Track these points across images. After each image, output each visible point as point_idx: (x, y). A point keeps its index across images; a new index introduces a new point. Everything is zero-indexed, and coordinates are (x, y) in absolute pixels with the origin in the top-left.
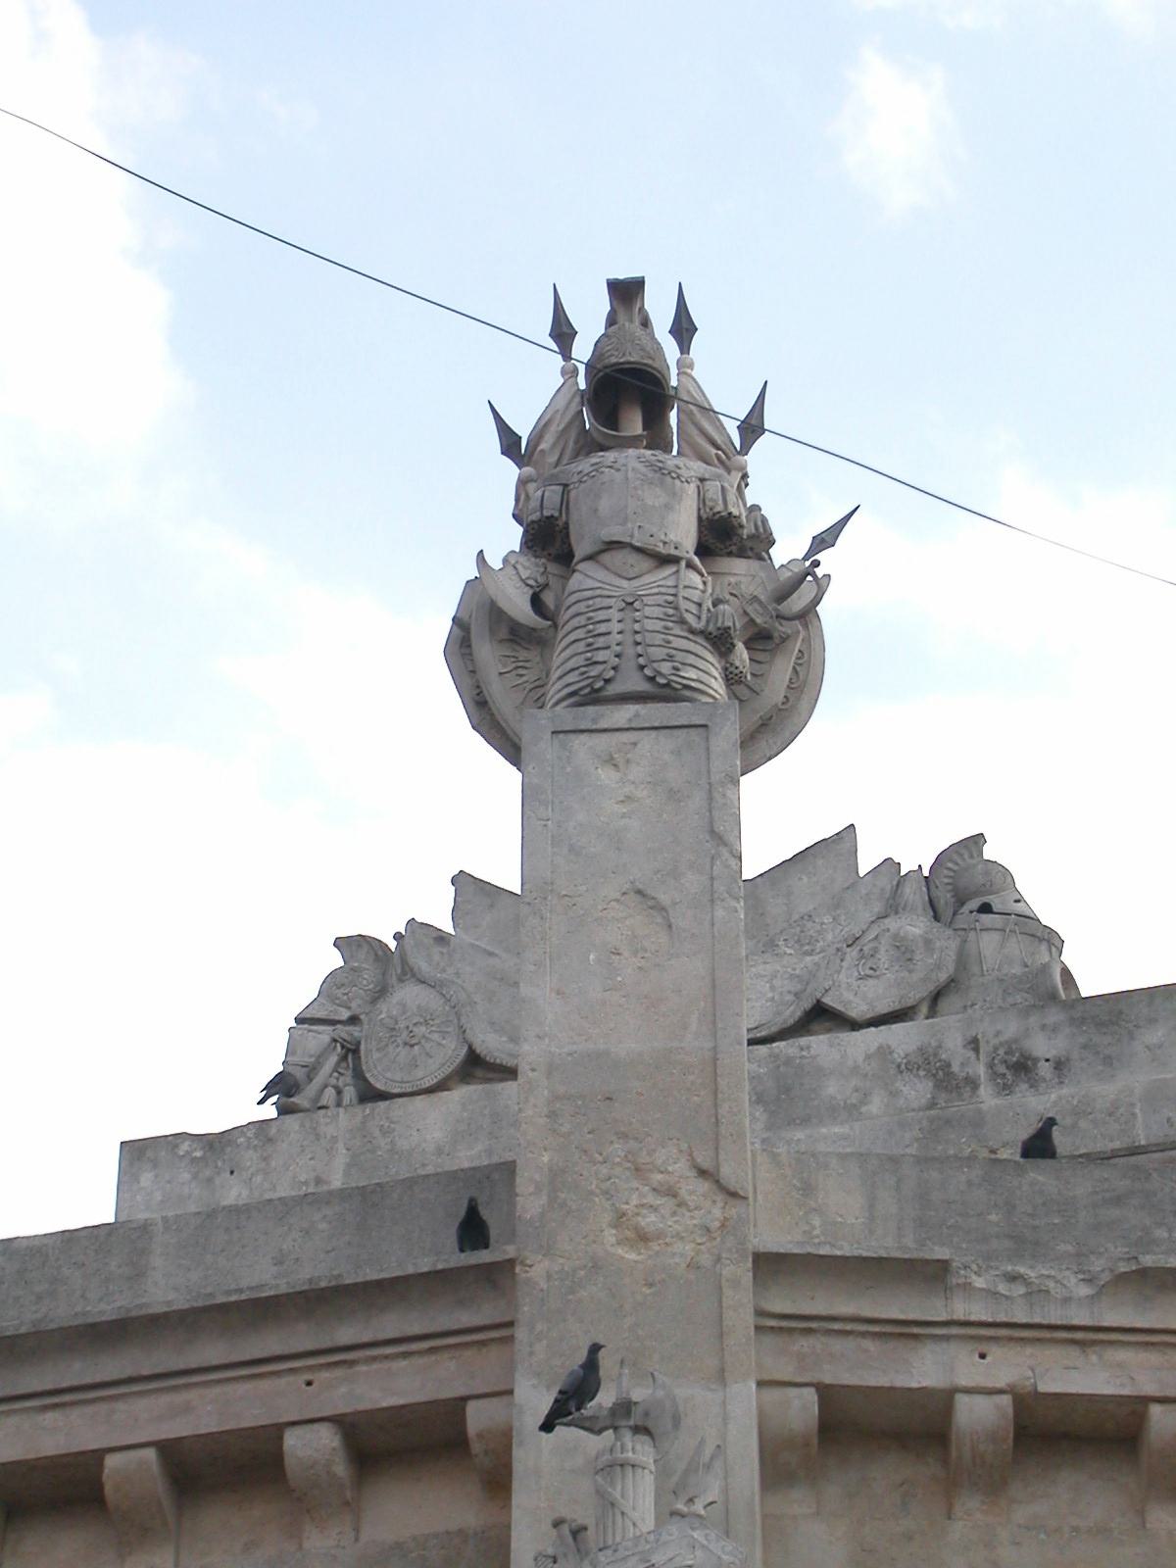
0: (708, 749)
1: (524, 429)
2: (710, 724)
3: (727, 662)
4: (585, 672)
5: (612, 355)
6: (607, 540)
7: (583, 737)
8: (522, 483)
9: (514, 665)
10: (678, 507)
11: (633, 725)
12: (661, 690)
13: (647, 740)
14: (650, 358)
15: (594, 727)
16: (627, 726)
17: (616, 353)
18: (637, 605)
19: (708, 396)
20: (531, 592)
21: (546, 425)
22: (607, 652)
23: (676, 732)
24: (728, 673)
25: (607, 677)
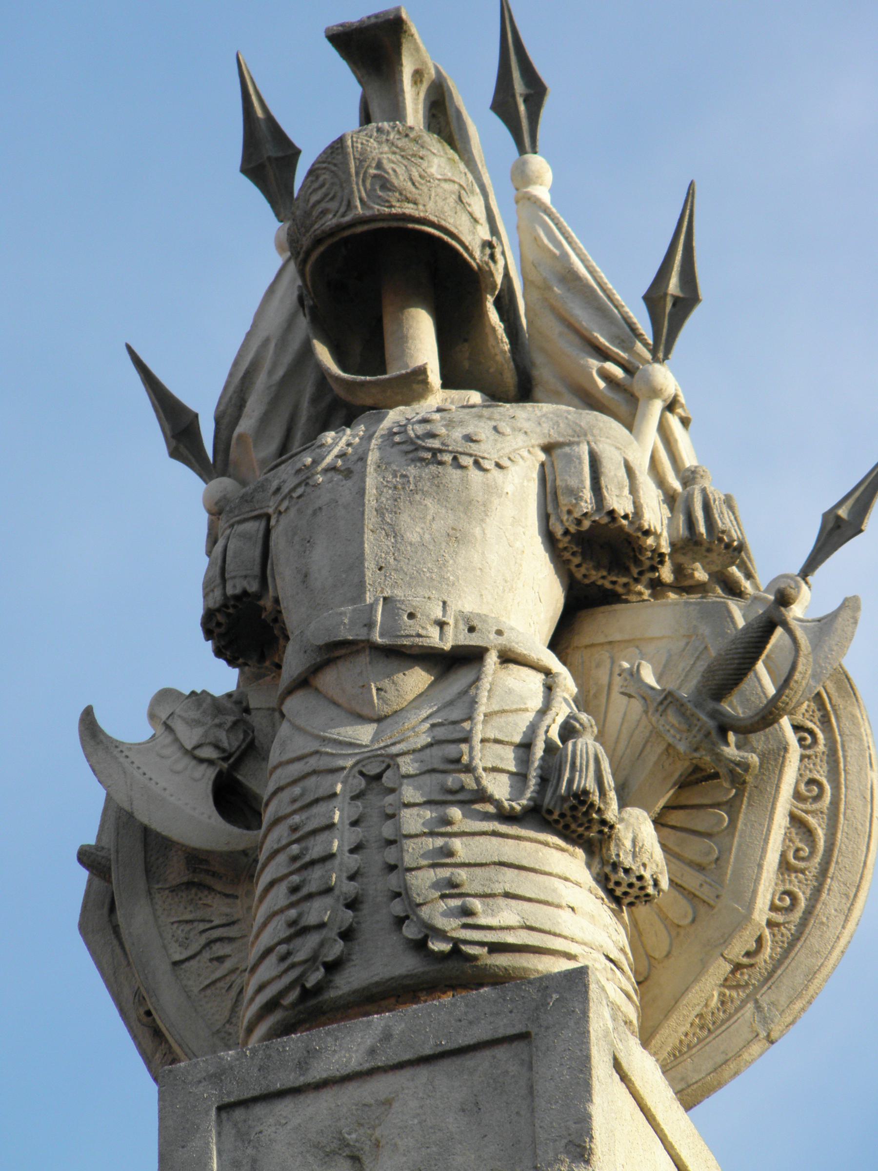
0: (531, 1090)
1: (203, 400)
2: (533, 1030)
3: (604, 862)
4: (289, 954)
5: (324, 212)
6: (321, 642)
7: (284, 1107)
8: (218, 511)
9: (203, 940)
10: (477, 531)
11: (381, 1060)
12: (437, 967)
13: (409, 1086)
14: (408, 200)
15: (302, 1080)
16: (367, 1066)
17: (333, 205)
18: (388, 780)
19: (685, 196)
20: (211, 773)
21: (520, 244)
22: (328, 900)
23: (469, 1061)
24: (611, 885)
25: (330, 958)
